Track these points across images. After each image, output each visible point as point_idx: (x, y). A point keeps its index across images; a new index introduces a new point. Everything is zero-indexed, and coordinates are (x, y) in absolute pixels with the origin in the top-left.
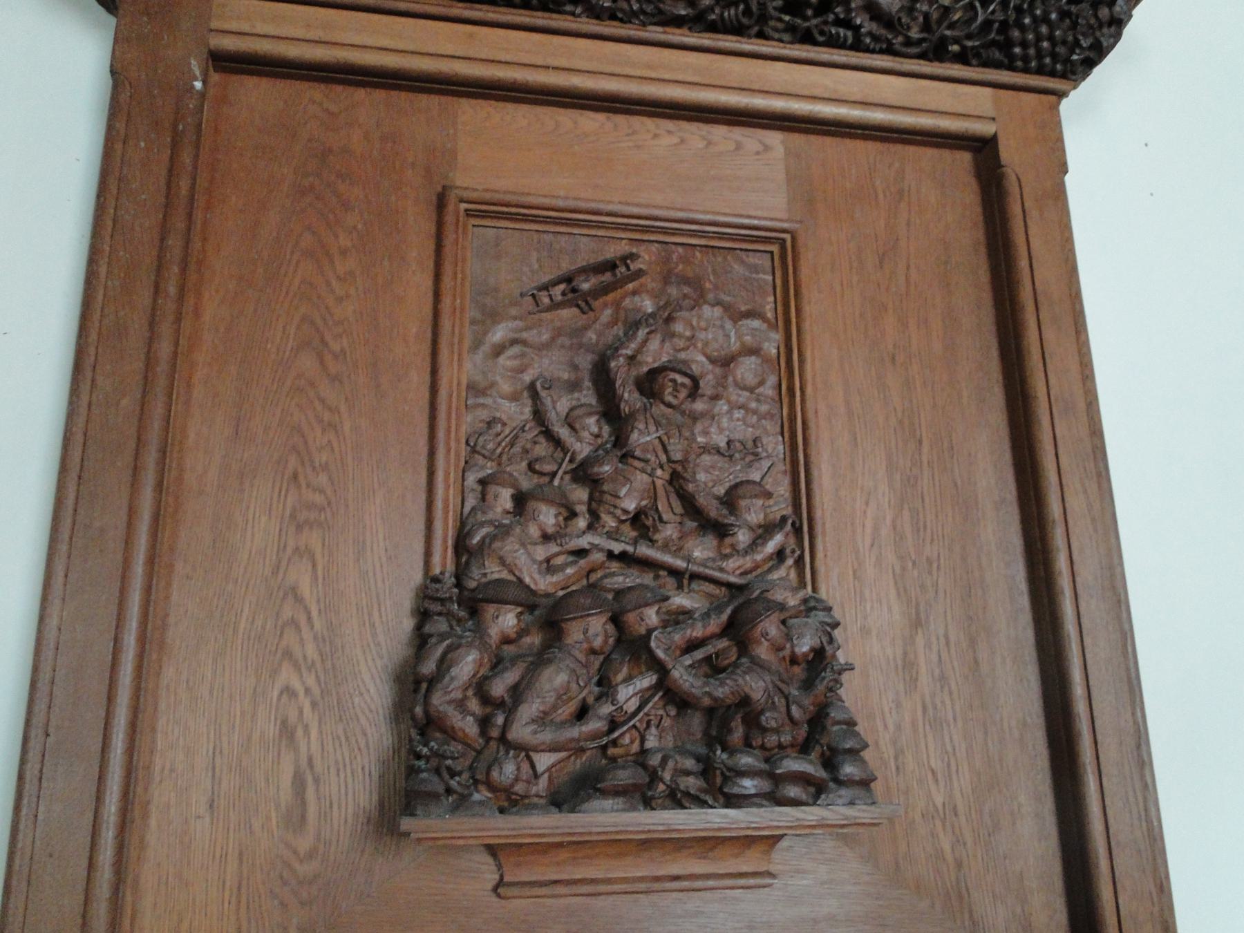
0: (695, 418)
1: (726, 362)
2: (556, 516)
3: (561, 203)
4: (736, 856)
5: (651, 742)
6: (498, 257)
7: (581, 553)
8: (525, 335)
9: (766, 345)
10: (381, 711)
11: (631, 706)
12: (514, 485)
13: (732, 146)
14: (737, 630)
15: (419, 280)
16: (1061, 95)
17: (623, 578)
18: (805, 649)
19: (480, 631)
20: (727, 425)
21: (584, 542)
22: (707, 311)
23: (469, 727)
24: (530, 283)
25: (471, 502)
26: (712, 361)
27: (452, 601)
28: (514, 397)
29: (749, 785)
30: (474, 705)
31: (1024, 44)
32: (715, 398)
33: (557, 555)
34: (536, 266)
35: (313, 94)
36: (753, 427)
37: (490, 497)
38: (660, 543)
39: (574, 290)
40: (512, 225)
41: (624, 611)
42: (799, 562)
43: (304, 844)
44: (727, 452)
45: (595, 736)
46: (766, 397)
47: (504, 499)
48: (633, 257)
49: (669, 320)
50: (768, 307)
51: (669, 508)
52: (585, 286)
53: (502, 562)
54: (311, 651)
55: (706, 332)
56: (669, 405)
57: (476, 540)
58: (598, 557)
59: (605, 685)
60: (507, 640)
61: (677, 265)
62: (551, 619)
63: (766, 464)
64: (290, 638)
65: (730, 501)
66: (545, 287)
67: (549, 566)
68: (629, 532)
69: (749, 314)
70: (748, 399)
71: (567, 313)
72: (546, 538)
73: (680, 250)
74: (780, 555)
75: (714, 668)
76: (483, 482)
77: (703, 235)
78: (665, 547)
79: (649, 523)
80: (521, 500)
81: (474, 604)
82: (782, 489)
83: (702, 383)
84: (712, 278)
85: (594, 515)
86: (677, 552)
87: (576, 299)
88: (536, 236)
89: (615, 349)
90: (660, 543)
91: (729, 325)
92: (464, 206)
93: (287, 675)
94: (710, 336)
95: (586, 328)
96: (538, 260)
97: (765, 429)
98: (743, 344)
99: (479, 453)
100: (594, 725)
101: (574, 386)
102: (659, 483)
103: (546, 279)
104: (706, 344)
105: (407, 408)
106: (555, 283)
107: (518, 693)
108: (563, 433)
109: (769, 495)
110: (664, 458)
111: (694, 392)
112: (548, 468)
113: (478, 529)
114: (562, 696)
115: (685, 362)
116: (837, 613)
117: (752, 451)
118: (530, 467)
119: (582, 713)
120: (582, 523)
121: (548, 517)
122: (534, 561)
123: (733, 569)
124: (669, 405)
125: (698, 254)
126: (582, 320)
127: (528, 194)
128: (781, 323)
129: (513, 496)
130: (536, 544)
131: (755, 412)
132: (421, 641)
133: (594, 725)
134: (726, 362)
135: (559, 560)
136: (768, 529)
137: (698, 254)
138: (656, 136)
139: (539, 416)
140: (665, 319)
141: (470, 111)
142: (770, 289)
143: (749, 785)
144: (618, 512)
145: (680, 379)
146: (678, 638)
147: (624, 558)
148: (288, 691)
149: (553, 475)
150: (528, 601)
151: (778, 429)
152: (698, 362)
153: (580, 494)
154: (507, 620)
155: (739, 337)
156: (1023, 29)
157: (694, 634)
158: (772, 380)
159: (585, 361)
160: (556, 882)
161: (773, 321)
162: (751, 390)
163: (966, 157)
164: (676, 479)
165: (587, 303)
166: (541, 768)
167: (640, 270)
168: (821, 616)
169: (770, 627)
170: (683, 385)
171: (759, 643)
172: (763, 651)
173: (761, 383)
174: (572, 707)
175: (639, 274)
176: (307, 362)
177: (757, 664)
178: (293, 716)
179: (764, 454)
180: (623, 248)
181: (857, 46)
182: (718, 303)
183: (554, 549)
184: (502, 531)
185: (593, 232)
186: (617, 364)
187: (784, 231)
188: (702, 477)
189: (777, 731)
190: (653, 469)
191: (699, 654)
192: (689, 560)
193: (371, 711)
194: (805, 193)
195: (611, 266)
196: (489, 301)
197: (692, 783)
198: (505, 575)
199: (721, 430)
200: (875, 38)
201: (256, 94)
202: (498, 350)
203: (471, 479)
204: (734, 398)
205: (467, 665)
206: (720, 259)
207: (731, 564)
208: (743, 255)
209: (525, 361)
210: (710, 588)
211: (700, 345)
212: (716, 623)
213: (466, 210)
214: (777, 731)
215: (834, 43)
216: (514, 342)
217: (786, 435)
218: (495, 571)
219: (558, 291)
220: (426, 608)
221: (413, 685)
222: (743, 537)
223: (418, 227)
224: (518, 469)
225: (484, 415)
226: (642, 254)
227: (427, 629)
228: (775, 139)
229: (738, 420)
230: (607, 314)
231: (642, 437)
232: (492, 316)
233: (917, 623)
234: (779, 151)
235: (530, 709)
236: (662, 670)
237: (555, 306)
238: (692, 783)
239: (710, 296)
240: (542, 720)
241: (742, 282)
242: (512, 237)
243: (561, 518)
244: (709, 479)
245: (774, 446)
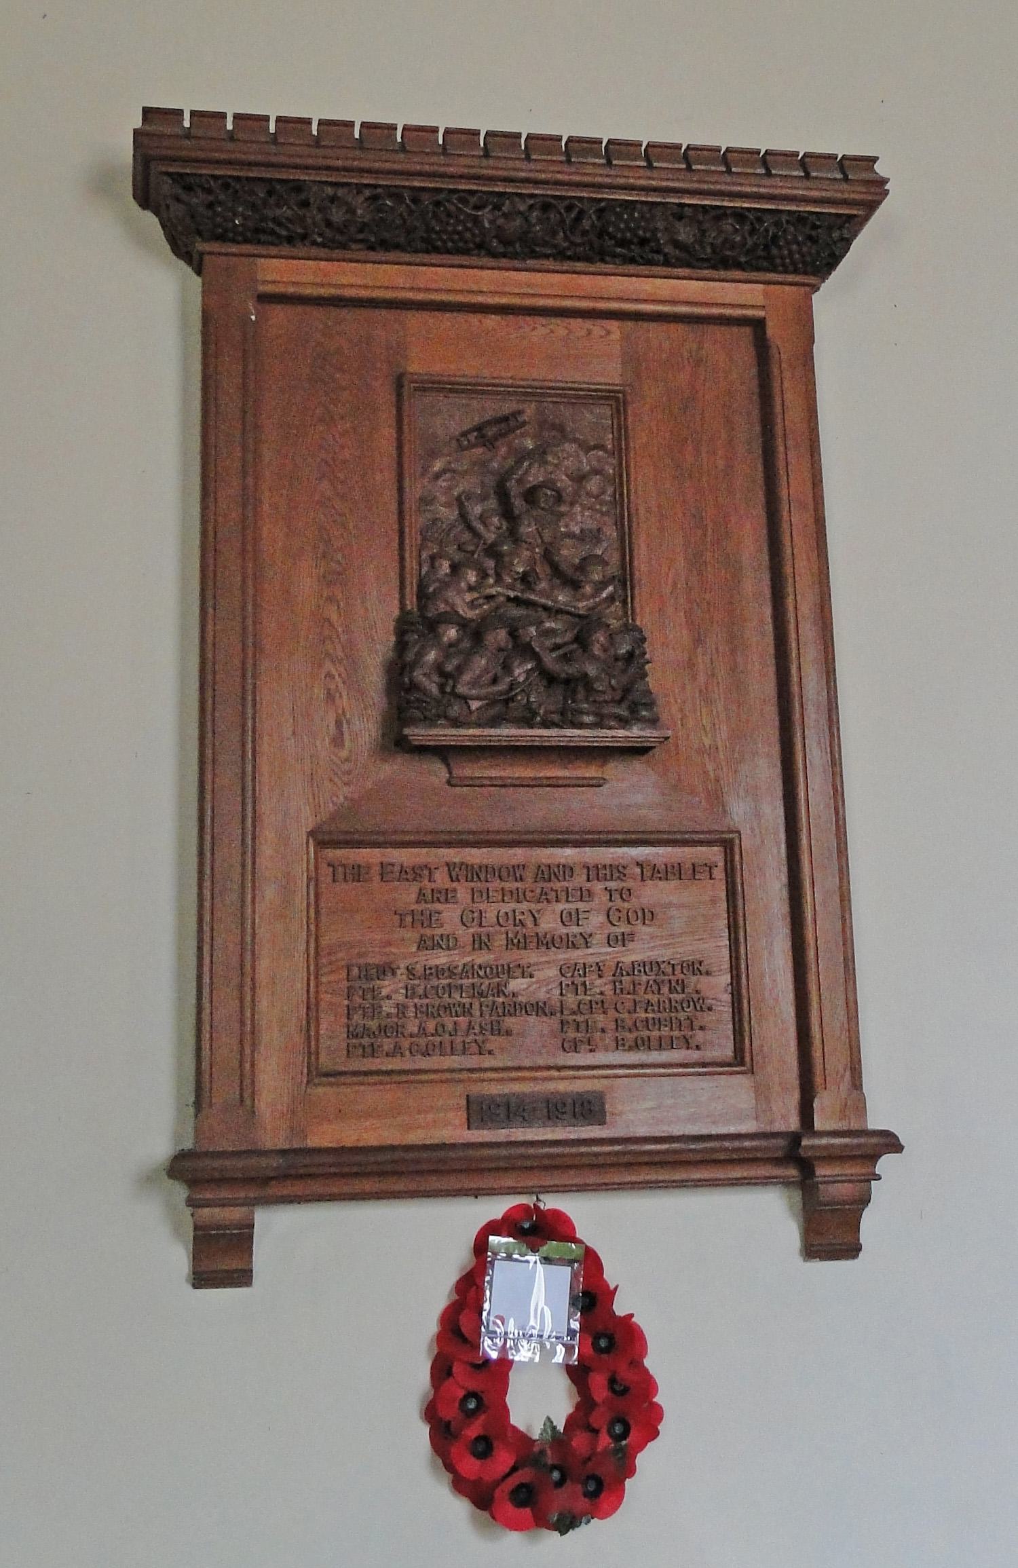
0: (562, 515)
1: (580, 479)
5: (532, 699)
7: (490, 598)
9: (607, 467)
11: (521, 679)
13: (583, 333)
14: (582, 641)
15: (388, 432)
16: (815, 288)
17: (516, 612)
18: (623, 651)
19: (438, 637)
20: (579, 519)
21: (493, 591)
23: (434, 690)
25: (425, 569)
26: (572, 479)
27: (417, 625)
28: (447, 505)
29: (588, 719)
30: (436, 678)
31: (782, 258)
32: (572, 504)
33: (477, 599)
35: (317, 313)
37: (437, 564)
41: (516, 630)
42: (624, 602)
43: (344, 753)
44: (582, 538)
45: (501, 693)
47: (445, 567)
48: (520, 412)
49: (544, 453)
51: (542, 569)
53: (447, 602)
54: (340, 654)
55: (567, 461)
56: (543, 509)
57: (431, 589)
58: (502, 599)
59: (507, 668)
60: (451, 645)
62: (475, 633)
63: (605, 544)
64: (329, 647)
65: (582, 567)
66: (464, 434)
67: (472, 605)
68: (518, 585)
69: (596, 447)
71: (480, 450)
72: (471, 588)
74: (611, 599)
75: (567, 658)
77: (565, 396)
78: (542, 593)
79: (531, 579)
80: (455, 568)
81: (433, 626)
82: (615, 559)
83: (564, 494)
86: (548, 598)
89: (511, 471)
91: (581, 453)
93: (328, 666)
95: (491, 460)
100: (502, 687)
101: (484, 498)
107: (460, 669)
108: (480, 527)
109: (607, 564)
110: (539, 541)
111: (559, 499)
112: (471, 548)
114: (486, 670)
116: (646, 634)
118: (460, 548)
119: (495, 681)
120: (491, 581)
121: (472, 577)
123: (582, 606)
124: (543, 509)
126: (489, 455)
132: (401, 646)
133: (502, 687)
134: (580, 479)
135: (481, 601)
136: (603, 585)
138: (534, 329)
139: (463, 516)
140: (540, 454)
141: (414, 319)
143: (588, 719)
146: (549, 643)
147: (516, 601)
148: (329, 675)
149: (473, 553)
150: (463, 624)
152: (563, 481)
153: (490, 564)
154: (452, 633)
155: (589, 462)
156: (780, 248)
158: (610, 491)
159: (490, 481)
162: (597, 497)
163: (747, 330)
164: (548, 556)
166: (473, 707)
168: (636, 634)
169: (600, 637)
172: (596, 650)
173: (603, 493)
174: (489, 676)
175: (524, 424)
176: (325, 485)
177: (594, 658)
178: (333, 687)
181: (667, 263)
182: (575, 440)
183: (476, 595)
184: (445, 585)
186: (512, 485)
187: (619, 392)
188: (564, 552)
189: (604, 692)
191: (561, 652)
192: (556, 601)
194: (633, 360)
195: (505, 419)
197: (556, 718)
198: (448, 609)
200: (678, 259)
201: (279, 315)
202: (437, 476)
203: (424, 555)
205: (432, 656)
207: (580, 605)
210: (566, 617)
212: (569, 636)
214: (604, 692)
215: (650, 263)
218: (442, 607)
220: (403, 627)
221: (399, 674)
222: (588, 589)
223: (384, 396)
224: (452, 549)
225: (429, 516)
227: (406, 638)
228: (613, 325)
230: (503, 450)
231: (527, 529)
232: (433, 454)
233: (698, 641)
234: (616, 336)
235: (466, 677)
236: (536, 657)
237: (472, 446)
238: (556, 718)
240: (474, 683)
244: (569, 554)
245: (611, 532)
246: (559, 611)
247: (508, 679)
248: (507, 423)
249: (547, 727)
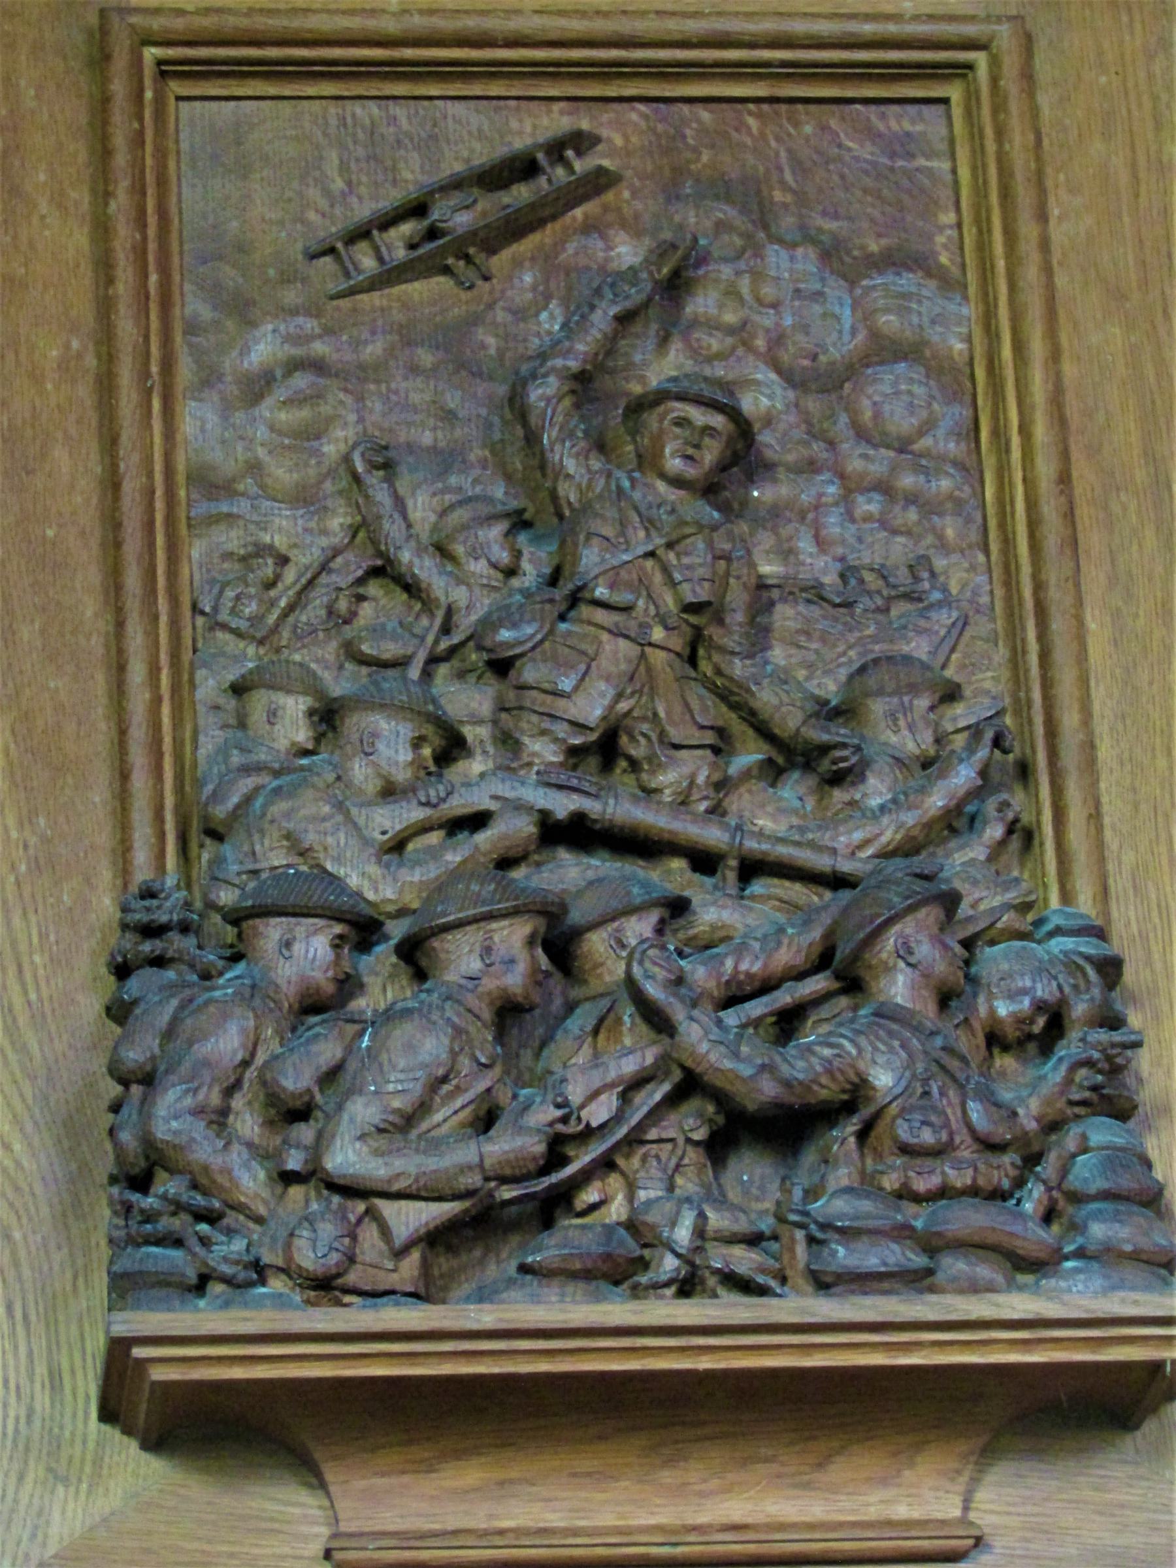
2: (417, 743)
3: (390, 26)
4: (884, 1482)
6: (244, 171)
8: (320, 348)
10: (39, 1189)
12: (313, 687)
14: (845, 970)
21: (480, 800)
22: (776, 258)
24: (328, 225)
28: (304, 498)
34: (339, 184)
36: (908, 533)
38: (667, 796)
39: (433, 233)
40: (272, 90)
44: (839, 601)
46: (942, 458)
47: (291, 719)
48: (581, 141)
50: (940, 239)
51: (683, 710)
52: (462, 221)
61: (696, 150)
66: (360, 234)
69: (890, 261)
70: (894, 469)
73: (705, 115)
76: (239, 689)
79: (638, 751)
80: (328, 717)
84: (788, 177)
85: (508, 741)
87: (442, 252)
88: (333, 109)
90: (667, 796)
91: (835, 289)
92: (151, 53)
94: (788, 321)
96: (344, 168)
97: (941, 537)
98: (875, 335)
99: (224, 627)
101: (446, 460)
102: (658, 658)
103: (363, 210)
104: (778, 340)
105: (50, 533)
106: (388, 222)
113: (232, 782)
115: (728, 387)
117: (912, 590)
119: (486, 1120)
122: (366, 842)
125: (752, 122)
127: (307, 11)
128: (972, 277)
129: (311, 713)
130: (369, 804)
131: (912, 499)
133: (511, 1144)
137: (752, 122)
142: (945, 194)
144: (561, 730)
145: (699, 416)
151: (974, 536)
157: (744, 966)
160: (455, 1533)
161: (955, 271)
165: (468, 258)
167: (600, 171)
170: (708, 430)
171: (889, 969)
175: (599, 183)
179: (936, 596)
180: (557, 122)
182: (808, 237)
185: (477, 89)
190: (644, 627)
193: (17, 1189)
195: (524, 168)
196: (229, 275)
199: (821, 543)
202: (257, 387)
203: (209, 686)
204: (855, 465)
206: (808, 129)
207: (844, 839)
208: (872, 111)
209: (326, 409)
211: (760, 343)
213: (160, 63)
216: (294, 366)
217: (995, 547)
219: (397, 241)
226: (604, 133)
229: (868, 518)
232: (242, 310)
235: (363, 1111)
239: (787, 223)
240: (403, 1125)
241: (869, 182)
242: (273, 121)
243: (427, 752)
246: (752, 869)
247: (544, 1114)
248: (528, 191)
249: (143, 142)
